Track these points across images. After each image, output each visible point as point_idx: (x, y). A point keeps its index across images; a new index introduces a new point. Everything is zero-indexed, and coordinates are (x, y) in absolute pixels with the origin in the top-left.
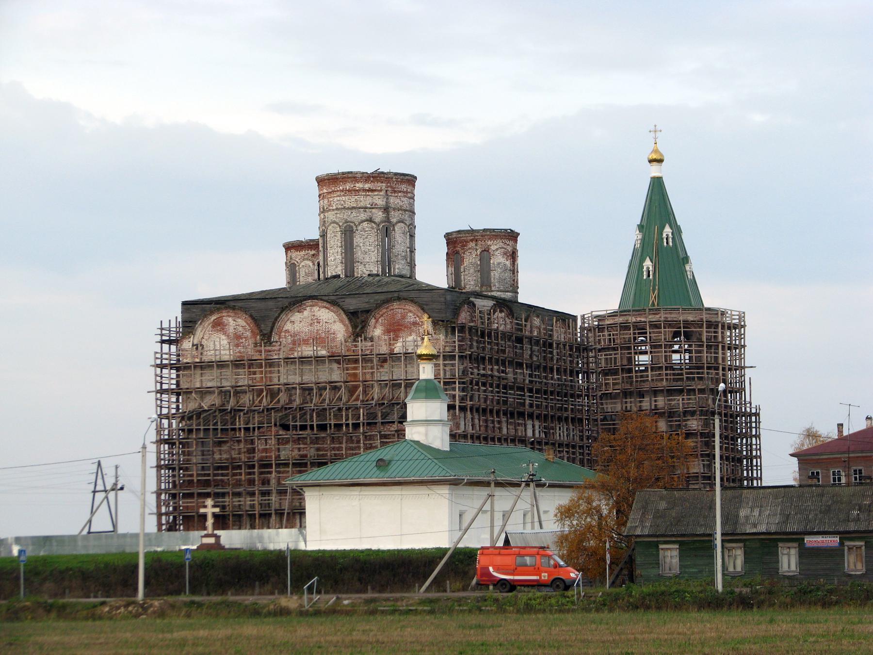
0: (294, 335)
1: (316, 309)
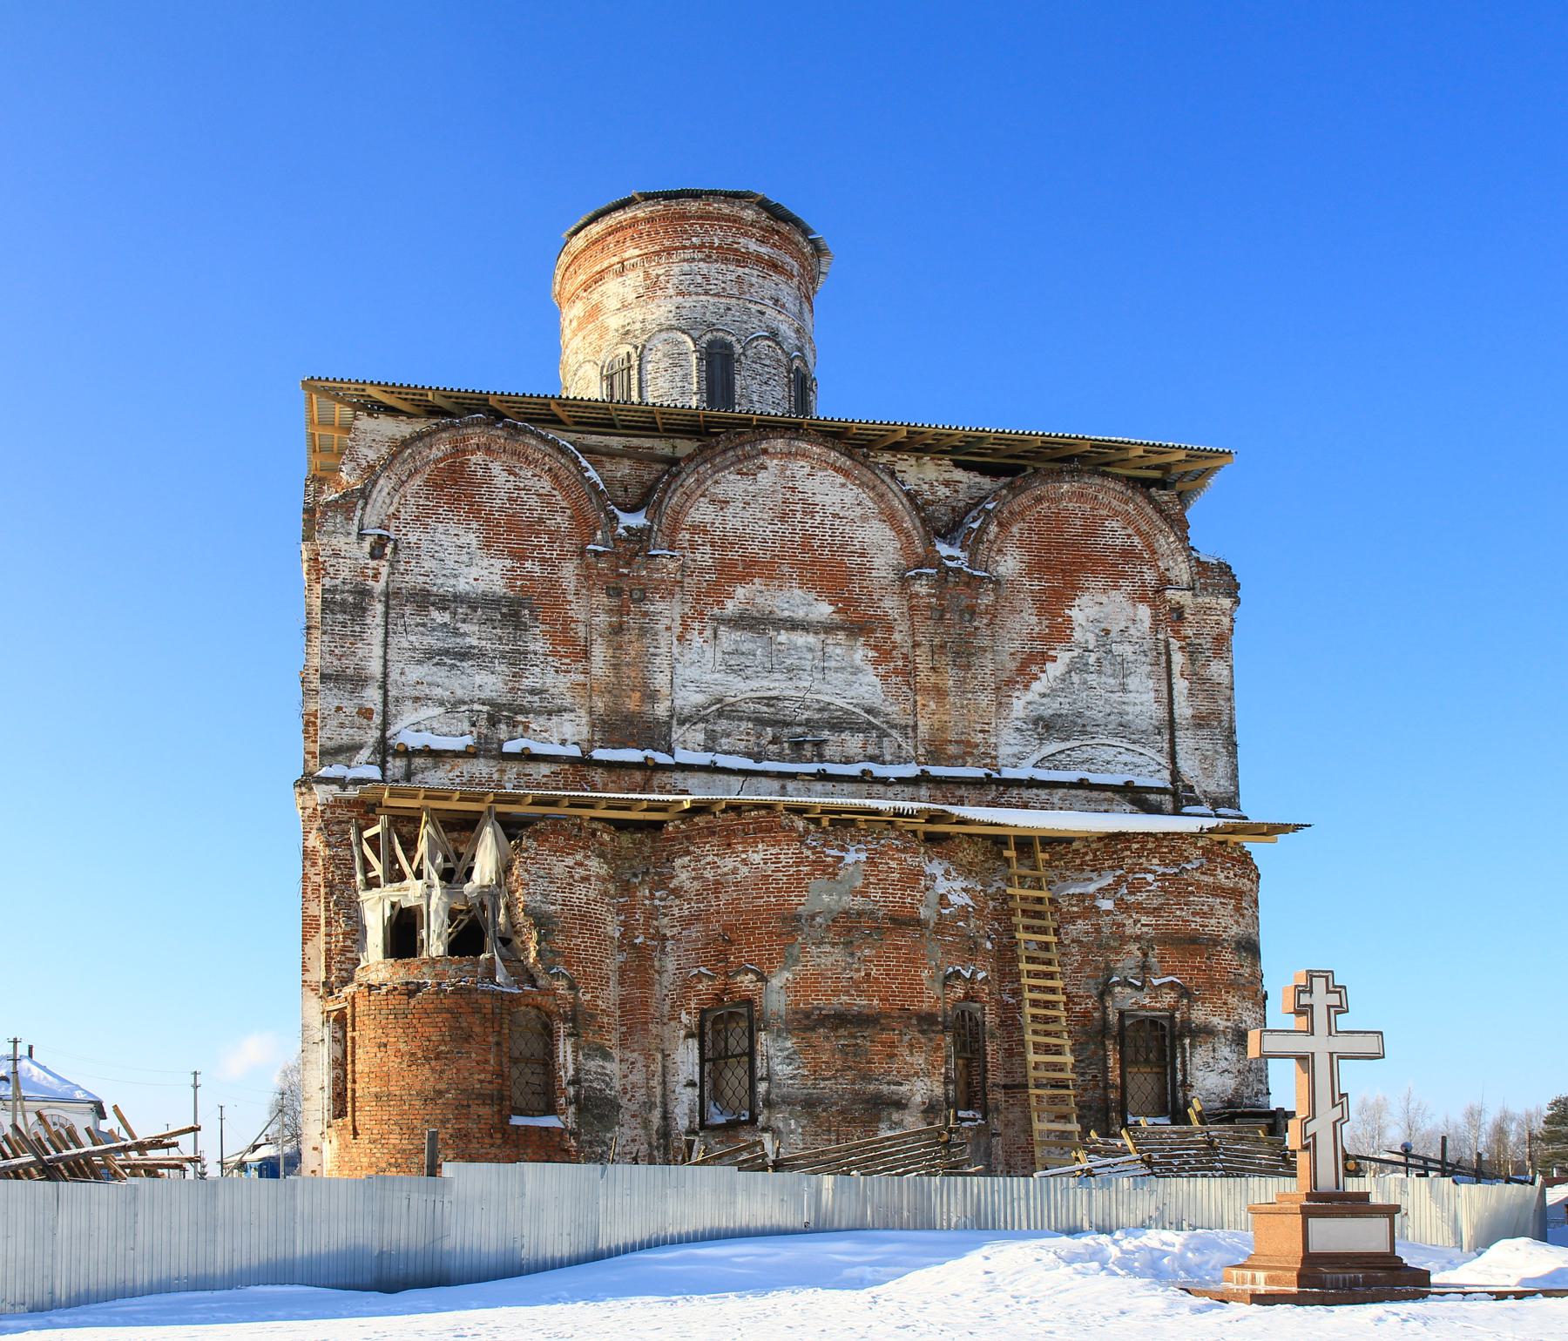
0: (723, 544)
1: (800, 468)
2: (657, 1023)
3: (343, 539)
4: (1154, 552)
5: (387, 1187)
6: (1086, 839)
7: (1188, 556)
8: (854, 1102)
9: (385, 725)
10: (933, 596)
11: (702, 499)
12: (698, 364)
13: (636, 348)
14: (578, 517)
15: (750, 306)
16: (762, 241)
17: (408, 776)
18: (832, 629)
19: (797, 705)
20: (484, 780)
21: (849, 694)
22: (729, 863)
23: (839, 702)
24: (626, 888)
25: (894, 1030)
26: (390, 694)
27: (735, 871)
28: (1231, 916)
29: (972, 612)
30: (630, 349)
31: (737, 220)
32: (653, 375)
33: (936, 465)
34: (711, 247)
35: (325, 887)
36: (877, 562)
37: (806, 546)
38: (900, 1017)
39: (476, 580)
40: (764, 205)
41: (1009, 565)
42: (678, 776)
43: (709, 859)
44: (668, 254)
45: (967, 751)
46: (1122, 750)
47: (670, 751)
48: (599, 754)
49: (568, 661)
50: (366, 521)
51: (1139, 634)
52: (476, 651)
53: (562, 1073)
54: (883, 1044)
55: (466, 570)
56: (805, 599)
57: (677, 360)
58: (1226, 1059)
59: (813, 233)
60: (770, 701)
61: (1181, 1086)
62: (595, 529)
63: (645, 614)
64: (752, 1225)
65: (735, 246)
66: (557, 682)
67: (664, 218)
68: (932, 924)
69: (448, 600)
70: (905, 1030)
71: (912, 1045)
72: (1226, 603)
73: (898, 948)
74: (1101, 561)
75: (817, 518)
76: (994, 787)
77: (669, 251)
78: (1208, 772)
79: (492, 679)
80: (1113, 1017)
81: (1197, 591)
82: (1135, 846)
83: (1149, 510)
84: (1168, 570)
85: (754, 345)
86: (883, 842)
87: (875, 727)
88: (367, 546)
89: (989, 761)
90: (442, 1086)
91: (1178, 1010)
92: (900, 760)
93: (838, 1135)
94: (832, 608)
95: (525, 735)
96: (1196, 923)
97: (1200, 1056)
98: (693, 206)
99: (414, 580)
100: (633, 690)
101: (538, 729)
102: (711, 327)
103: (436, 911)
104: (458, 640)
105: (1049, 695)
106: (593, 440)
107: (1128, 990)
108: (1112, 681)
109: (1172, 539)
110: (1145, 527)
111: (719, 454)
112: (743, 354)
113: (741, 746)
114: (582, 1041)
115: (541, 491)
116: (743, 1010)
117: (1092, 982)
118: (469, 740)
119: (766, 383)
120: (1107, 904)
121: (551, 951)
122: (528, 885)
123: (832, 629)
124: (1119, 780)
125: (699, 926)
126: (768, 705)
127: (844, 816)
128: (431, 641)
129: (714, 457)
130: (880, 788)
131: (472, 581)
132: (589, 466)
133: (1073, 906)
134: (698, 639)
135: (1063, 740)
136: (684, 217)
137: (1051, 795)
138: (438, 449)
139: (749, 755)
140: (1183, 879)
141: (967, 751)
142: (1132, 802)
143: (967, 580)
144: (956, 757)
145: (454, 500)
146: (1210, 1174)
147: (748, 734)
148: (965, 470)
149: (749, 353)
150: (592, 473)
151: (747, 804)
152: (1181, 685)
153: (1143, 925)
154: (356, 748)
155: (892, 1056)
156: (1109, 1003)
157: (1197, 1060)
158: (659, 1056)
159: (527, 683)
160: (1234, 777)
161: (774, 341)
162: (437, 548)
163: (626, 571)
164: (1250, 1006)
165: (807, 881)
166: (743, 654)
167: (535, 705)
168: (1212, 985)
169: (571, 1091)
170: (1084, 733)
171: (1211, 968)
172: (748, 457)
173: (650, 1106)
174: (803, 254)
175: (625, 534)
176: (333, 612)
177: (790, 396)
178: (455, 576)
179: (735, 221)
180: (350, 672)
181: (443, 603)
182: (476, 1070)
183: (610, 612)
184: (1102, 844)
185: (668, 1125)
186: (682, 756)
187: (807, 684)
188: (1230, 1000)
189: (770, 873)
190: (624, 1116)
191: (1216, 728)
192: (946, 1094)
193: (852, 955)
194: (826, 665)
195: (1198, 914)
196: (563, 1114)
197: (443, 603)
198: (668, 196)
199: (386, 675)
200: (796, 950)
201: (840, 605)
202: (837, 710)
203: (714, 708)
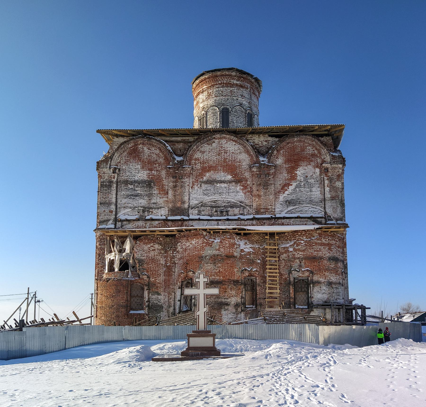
0: (204, 162)
1: (224, 141)
2: (173, 285)
3: (106, 169)
4: (320, 154)
5: (9, 334)
6: (288, 232)
7: (329, 154)
8: (215, 304)
9: (116, 214)
10: (258, 171)
11: (198, 152)
12: (219, 114)
13: (205, 112)
14: (166, 159)
15: (234, 98)
16: (238, 80)
17: (122, 226)
18: (231, 182)
19: (222, 202)
20: (141, 226)
21: (236, 198)
22: (188, 244)
23: (233, 200)
24: (166, 252)
25: (226, 285)
26: (118, 206)
27: (189, 246)
28: (327, 251)
29: (269, 174)
30: (204, 112)
31: (230, 75)
32: (209, 118)
33: (264, 136)
34: (224, 83)
35: (98, 255)
36: (244, 164)
37: (225, 161)
38: (228, 281)
39: (140, 177)
40: (238, 70)
41: (280, 161)
42: (191, 222)
43: (184, 243)
44: (213, 86)
45: (267, 210)
46: (311, 207)
47: (188, 216)
48: (170, 218)
49: (163, 195)
50: (112, 164)
51: (316, 176)
52: (140, 194)
53: (145, 299)
54: (223, 289)
55: (137, 174)
56: (224, 175)
57: (214, 114)
58: (324, 290)
59: (254, 76)
60: (215, 202)
61: (310, 297)
62: (170, 162)
63: (182, 182)
64: (109, 340)
65: (230, 82)
66: (159, 200)
67: (212, 77)
68: (238, 257)
69: (133, 182)
70: (229, 285)
71: (231, 289)
72: (341, 166)
73: (228, 263)
74: (306, 158)
75: (228, 154)
76: (274, 220)
77: (213, 86)
78: (335, 212)
79: (144, 201)
80: (292, 279)
81: (332, 163)
82: (299, 234)
83: (319, 143)
84: (325, 158)
85: (235, 108)
86: (225, 237)
87: (242, 206)
88: (111, 170)
89: (272, 213)
90: (113, 304)
91: (310, 277)
92: (249, 214)
93: (211, 313)
94: (231, 177)
95: (152, 214)
96: (315, 253)
97: (316, 289)
98: (219, 73)
99: (123, 177)
100: (179, 201)
101: (155, 212)
102: (223, 105)
103: (117, 260)
104: (135, 192)
105: (290, 194)
106: (168, 139)
107: (296, 272)
108: (308, 189)
109: (325, 150)
110: (318, 148)
111: (202, 140)
112: (232, 111)
113: (207, 213)
114: (151, 291)
115: (157, 153)
116: (190, 281)
117: (287, 270)
118: (137, 217)
119: (238, 117)
120: (291, 249)
121: (143, 269)
122: (137, 252)
123: (231, 182)
124: (309, 215)
125: (182, 260)
126: (214, 203)
127: (216, 230)
128: (128, 193)
129: (201, 141)
130: (243, 222)
131: (139, 177)
132: (169, 146)
133: (282, 250)
134: (196, 187)
135: (294, 206)
136: (217, 76)
137: (290, 220)
138: (131, 145)
139: (209, 215)
140: (311, 242)
141: (267, 210)
142: (313, 221)
143: (267, 166)
144: (263, 213)
145: (134, 157)
146: (282, 322)
147: (209, 210)
148: (272, 137)
149: (233, 110)
150: (169, 148)
151: (193, 229)
152: (327, 189)
153: (300, 255)
154: (108, 220)
155: (225, 292)
156: (291, 276)
157: (315, 290)
158: (173, 294)
159: (152, 201)
160: (343, 212)
161: (240, 106)
162: (130, 170)
163: (177, 172)
164: (334, 275)
165: (205, 248)
166: (208, 190)
167: (154, 207)
168: (320, 270)
169: (147, 304)
170: (300, 204)
171: (319, 265)
172: (210, 140)
173: (169, 306)
174: (252, 82)
175: (177, 162)
176: (103, 187)
177: (246, 120)
178: (135, 176)
179: (230, 76)
180: (107, 202)
181: (132, 183)
182: (122, 300)
183: (173, 182)
184: (292, 233)
185: (175, 311)
186: (191, 217)
187: (224, 197)
188: (326, 274)
189: (196, 246)
190: (164, 310)
191: (337, 200)
192: (241, 301)
193: (215, 266)
194: (229, 191)
195: (316, 251)
196: (145, 310)
197: (132, 183)
198: (212, 71)
199: (116, 202)
200: (202, 266)
201: (234, 176)
202: (232, 203)
203: (200, 204)
